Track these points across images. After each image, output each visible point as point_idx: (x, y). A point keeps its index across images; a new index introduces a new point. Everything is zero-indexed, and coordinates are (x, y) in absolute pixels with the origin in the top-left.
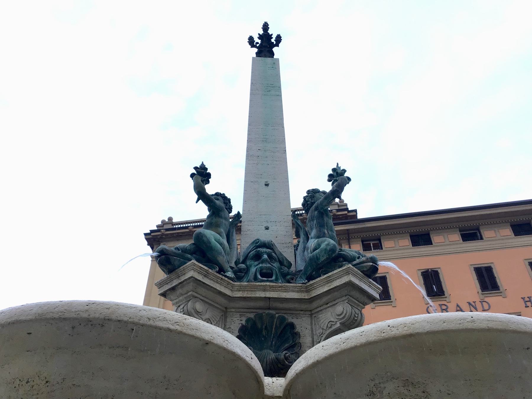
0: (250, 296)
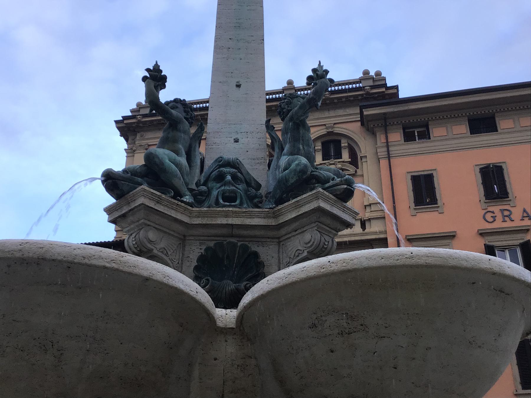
0: (210, 223)
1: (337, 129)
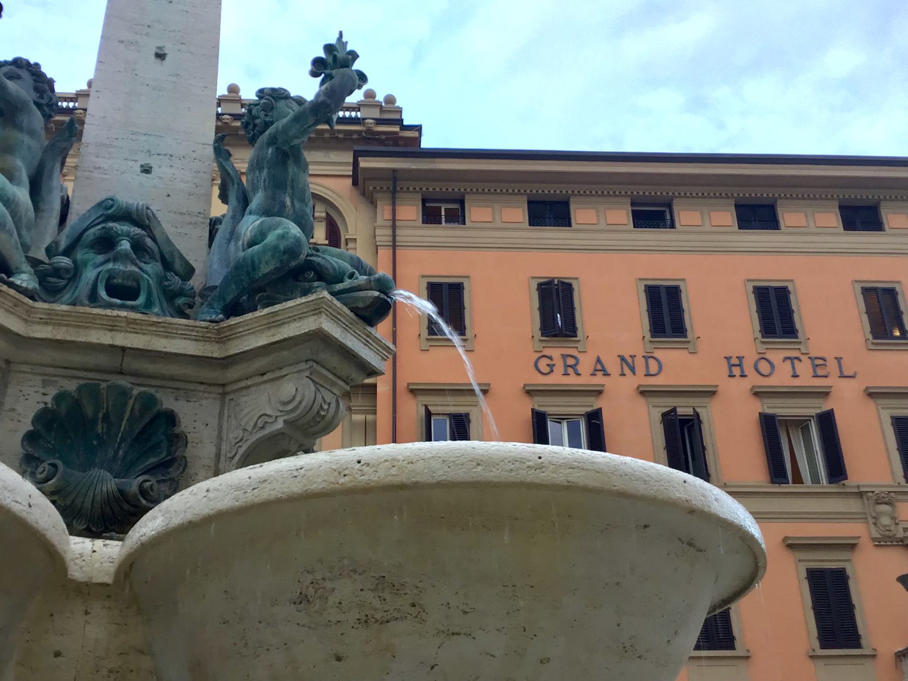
0: (73, 339)
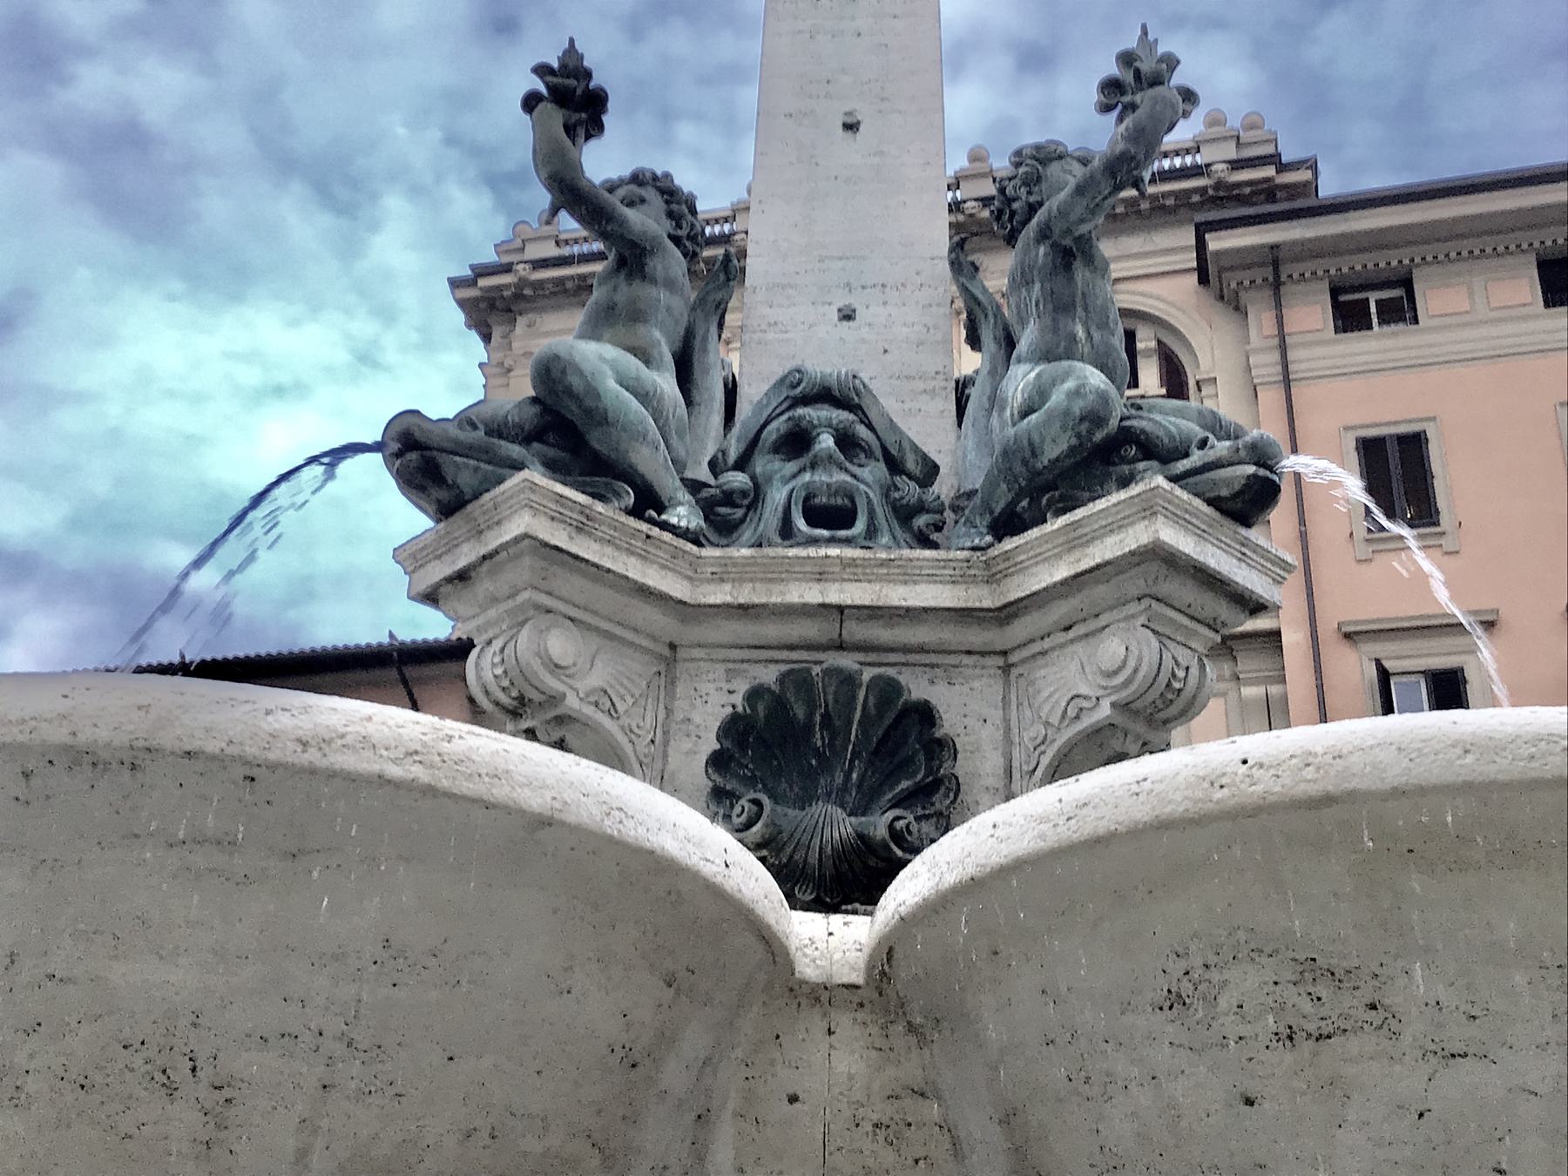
0: (763, 600)
1: (1127, 297)
